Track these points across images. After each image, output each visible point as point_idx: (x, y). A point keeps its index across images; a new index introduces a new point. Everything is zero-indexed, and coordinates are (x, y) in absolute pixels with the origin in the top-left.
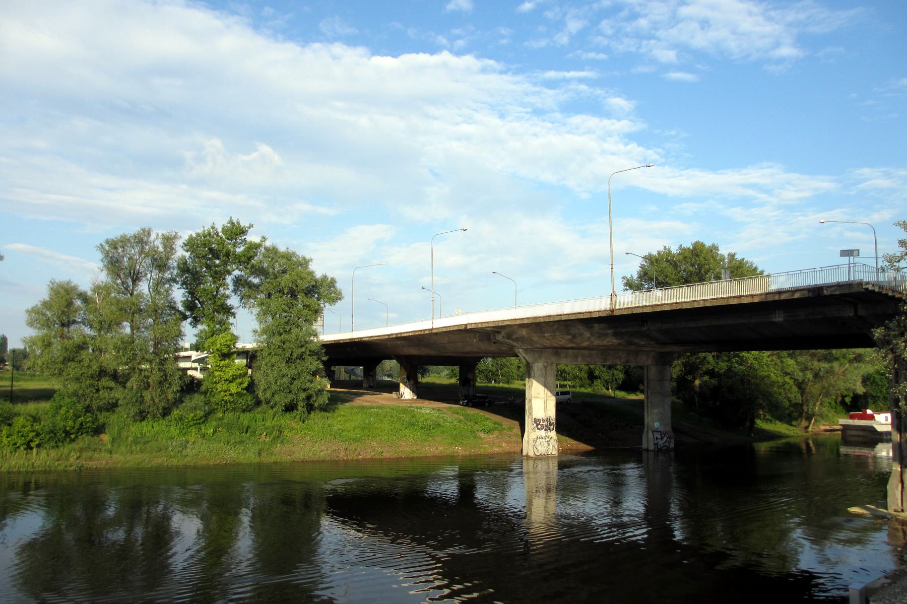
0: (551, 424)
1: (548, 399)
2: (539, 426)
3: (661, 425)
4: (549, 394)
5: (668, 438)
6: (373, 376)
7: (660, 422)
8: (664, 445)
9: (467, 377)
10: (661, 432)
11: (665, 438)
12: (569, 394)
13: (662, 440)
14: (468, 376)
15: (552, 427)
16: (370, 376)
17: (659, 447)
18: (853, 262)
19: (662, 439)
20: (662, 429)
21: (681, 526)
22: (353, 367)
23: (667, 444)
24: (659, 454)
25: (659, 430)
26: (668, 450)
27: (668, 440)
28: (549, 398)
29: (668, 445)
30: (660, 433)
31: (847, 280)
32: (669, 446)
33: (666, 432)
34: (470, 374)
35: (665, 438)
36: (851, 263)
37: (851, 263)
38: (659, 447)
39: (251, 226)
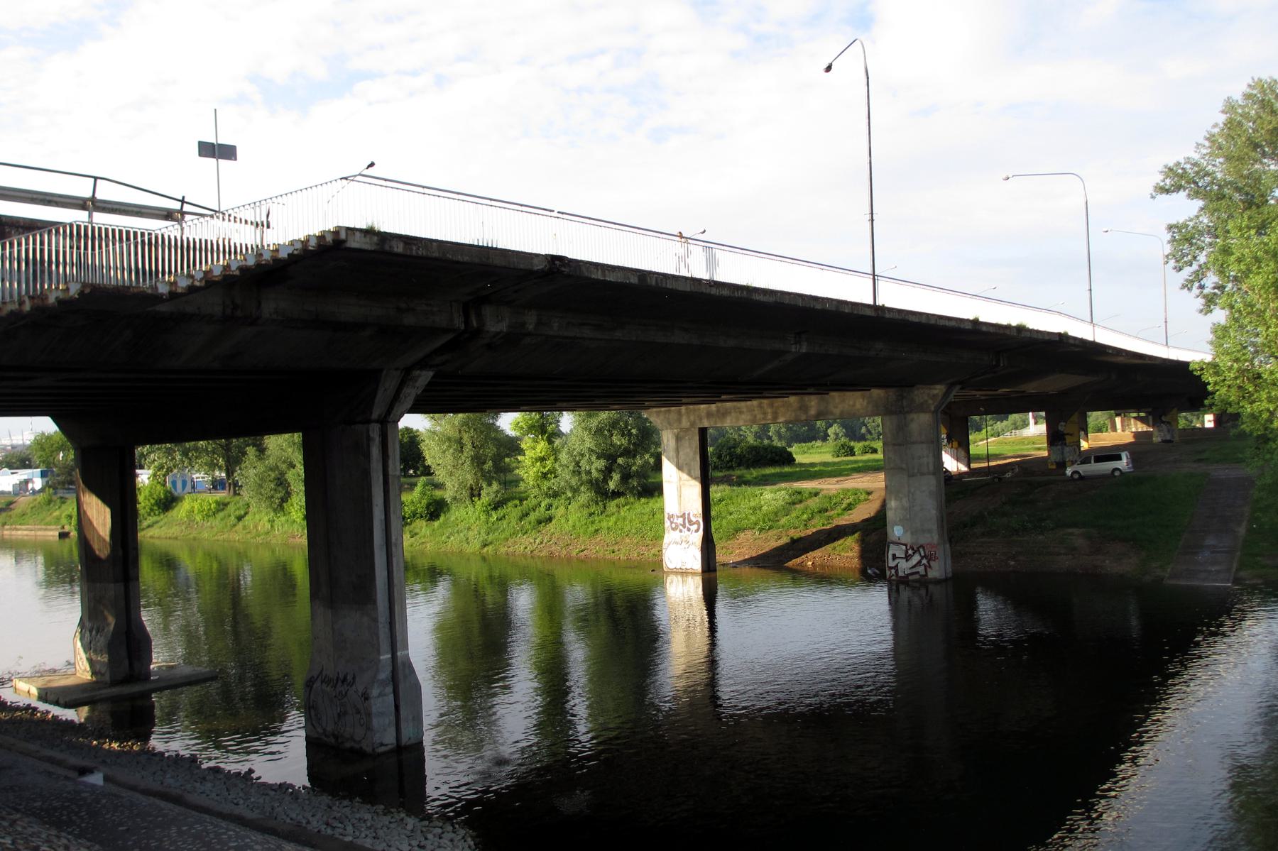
0: (691, 522)
1: (684, 484)
2: (674, 526)
3: (905, 531)
4: (685, 476)
5: (922, 558)
6: (1169, 423)
7: (903, 526)
8: (914, 570)
9: (1058, 430)
10: (906, 545)
11: (916, 558)
12: (1095, 457)
13: (907, 561)
14: (1060, 428)
15: (695, 527)
16: (1163, 422)
17: (901, 574)
18: (184, 210)
19: (907, 558)
20: (907, 539)
21: (657, 677)
22: (708, 437)
23: (921, 569)
24: (902, 587)
25: (903, 541)
26: (924, 582)
27: (924, 561)
28: (686, 483)
29: (923, 573)
30: (904, 547)
31: (115, 284)
32: (926, 575)
33: (922, 546)
34: (1063, 423)
35: (916, 558)
36: (185, 205)
37: (185, 205)
38: (901, 574)
39: (199, 308)
